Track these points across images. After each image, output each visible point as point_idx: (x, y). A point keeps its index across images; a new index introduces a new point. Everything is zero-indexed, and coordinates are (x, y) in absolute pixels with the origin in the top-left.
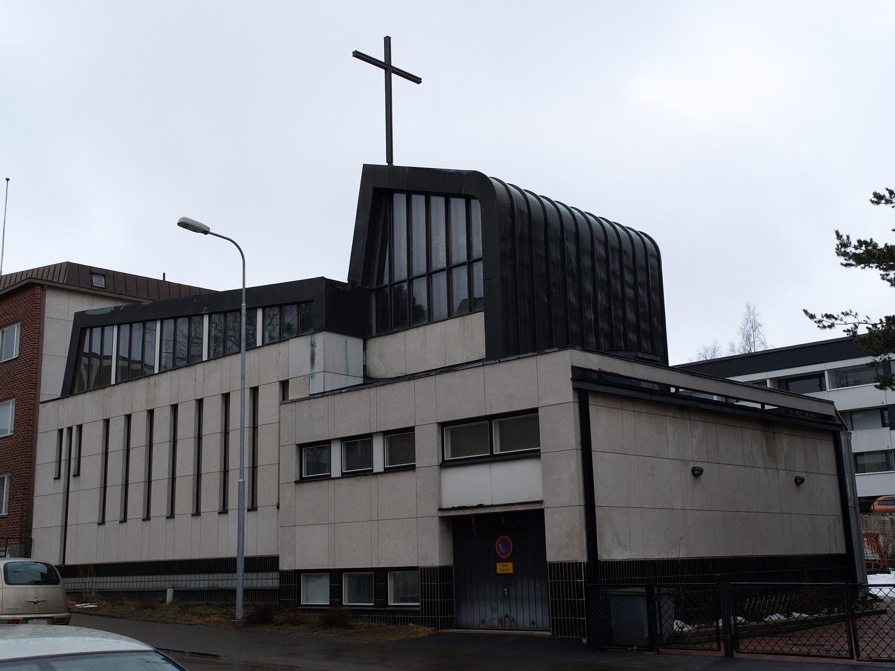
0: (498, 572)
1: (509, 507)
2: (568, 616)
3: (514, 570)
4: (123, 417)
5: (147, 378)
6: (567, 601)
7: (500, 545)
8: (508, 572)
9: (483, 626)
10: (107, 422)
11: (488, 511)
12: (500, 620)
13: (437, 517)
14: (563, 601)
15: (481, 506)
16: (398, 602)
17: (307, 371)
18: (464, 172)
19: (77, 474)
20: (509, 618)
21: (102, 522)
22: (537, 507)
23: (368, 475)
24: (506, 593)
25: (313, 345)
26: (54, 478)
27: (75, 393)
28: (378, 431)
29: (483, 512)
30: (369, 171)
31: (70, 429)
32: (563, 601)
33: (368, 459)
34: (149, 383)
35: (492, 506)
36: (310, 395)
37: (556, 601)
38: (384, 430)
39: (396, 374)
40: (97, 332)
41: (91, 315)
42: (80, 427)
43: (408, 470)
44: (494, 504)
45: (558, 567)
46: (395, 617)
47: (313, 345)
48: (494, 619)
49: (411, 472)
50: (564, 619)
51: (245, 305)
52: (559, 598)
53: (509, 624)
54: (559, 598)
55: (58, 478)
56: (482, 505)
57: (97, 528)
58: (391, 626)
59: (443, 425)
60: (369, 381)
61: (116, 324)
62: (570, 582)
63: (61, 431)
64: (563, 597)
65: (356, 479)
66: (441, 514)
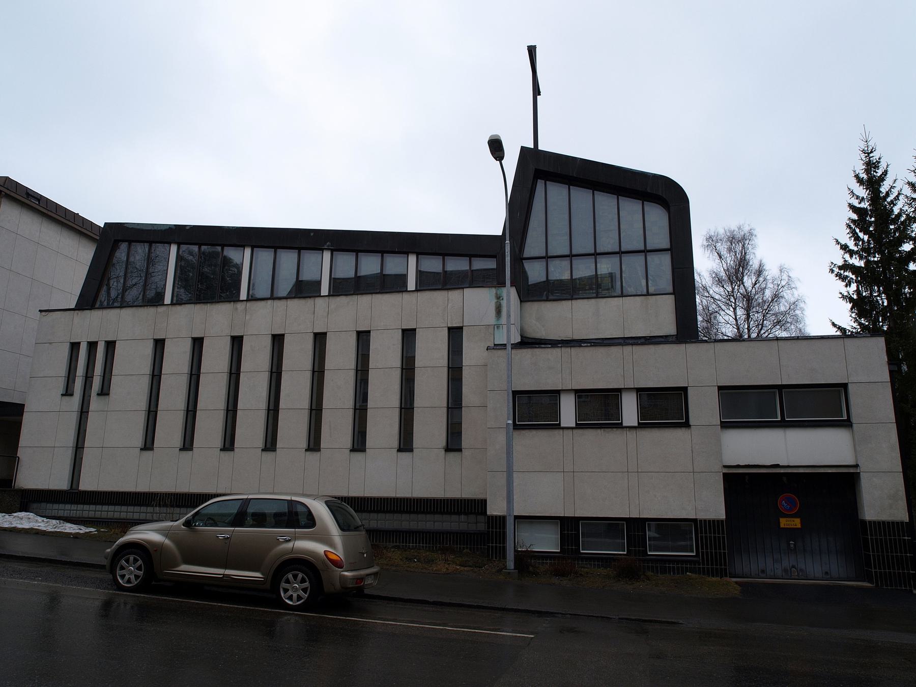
0: (781, 526)
1: (816, 469)
2: (894, 569)
3: (801, 525)
4: (86, 342)
5: (232, 303)
6: (892, 556)
7: (784, 502)
8: (795, 527)
9: (763, 575)
10: (159, 344)
11: (782, 471)
12: (785, 571)
13: (722, 473)
14: (888, 556)
15: (777, 466)
16: (654, 551)
17: (491, 319)
18: (649, 174)
19: (104, 392)
20: (796, 569)
21: (148, 445)
22: (852, 470)
23: (614, 428)
24: (792, 546)
25: (500, 297)
26: (62, 395)
27: (96, 307)
28: (625, 387)
29: (782, 472)
30: (524, 150)
31: (92, 346)
32: (888, 556)
33: (555, 413)
34: (236, 309)
35: (788, 467)
36: (495, 345)
37: (878, 556)
38: (576, 388)
39: (560, 337)
40: (124, 246)
41: (132, 228)
42: (111, 346)
43: (600, 428)
44: (791, 464)
45: (880, 528)
46: (666, 566)
47: (499, 298)
48: (777, 569)
49: (683, 429)
50: (890, 573)
51: (509, 242)
52: (883, 552)
53: (796, 574)
54: (883, 552)
55: (68, 393)
56: (779, 465)
57: (260, 453)
58: (596, 569)
59: (720, 388)
60: (527, 342)
61: (175, 243)
62: (895, 540)
63: (75, 346)
64: (887, 552)
65: (604, 430)
66: (726, 471)
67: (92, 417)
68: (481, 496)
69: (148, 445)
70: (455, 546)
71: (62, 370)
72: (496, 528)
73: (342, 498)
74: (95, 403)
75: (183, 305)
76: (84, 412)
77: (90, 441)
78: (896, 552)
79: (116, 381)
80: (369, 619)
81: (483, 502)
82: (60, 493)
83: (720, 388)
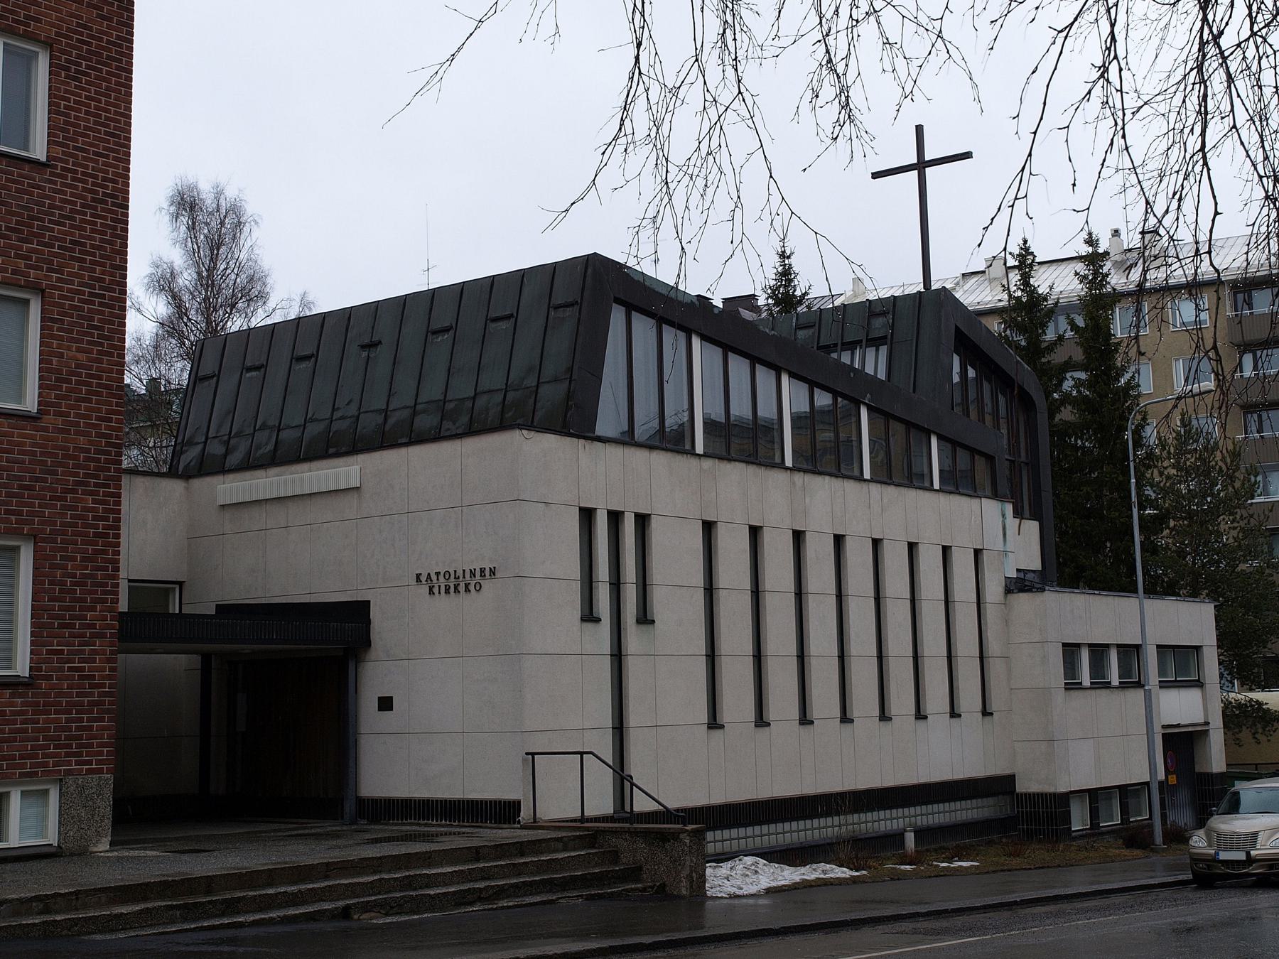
15: (1178, 726)
19: (645, 619)
29: (1190, 730)
31: (615, 518)
42: (642, 521)
55: (589, 616)
59: (1064, 645)
63: (587, 515)
67: (633, 666)
68: (1008, 772)
69: (714, 723)
70: (1203, 787)
71: (574, 568)
72: (1026, 808)
73: (678, 810)
74: (634, 638)
75: (733, 463)
76: (618, 657)
77: (634, 718)
78: (1031, 825)
79: (658, 596)
80: (877, 956)
81: (1012, 778)
82: (750, 805)
83: (1064, 645)
